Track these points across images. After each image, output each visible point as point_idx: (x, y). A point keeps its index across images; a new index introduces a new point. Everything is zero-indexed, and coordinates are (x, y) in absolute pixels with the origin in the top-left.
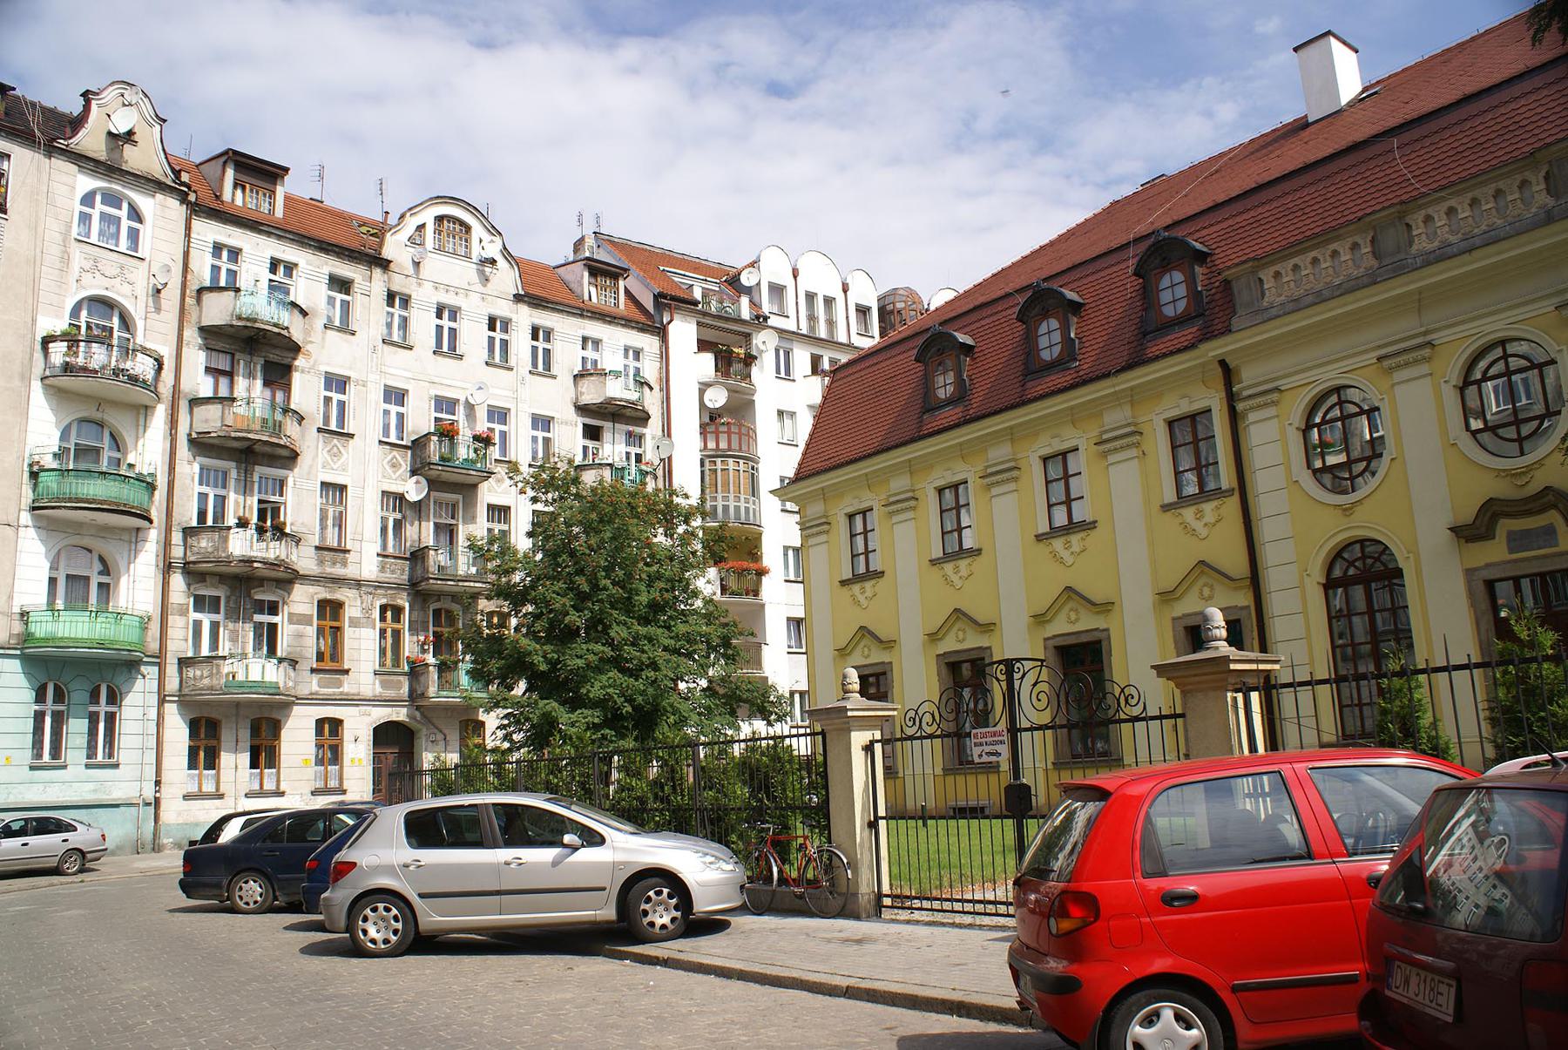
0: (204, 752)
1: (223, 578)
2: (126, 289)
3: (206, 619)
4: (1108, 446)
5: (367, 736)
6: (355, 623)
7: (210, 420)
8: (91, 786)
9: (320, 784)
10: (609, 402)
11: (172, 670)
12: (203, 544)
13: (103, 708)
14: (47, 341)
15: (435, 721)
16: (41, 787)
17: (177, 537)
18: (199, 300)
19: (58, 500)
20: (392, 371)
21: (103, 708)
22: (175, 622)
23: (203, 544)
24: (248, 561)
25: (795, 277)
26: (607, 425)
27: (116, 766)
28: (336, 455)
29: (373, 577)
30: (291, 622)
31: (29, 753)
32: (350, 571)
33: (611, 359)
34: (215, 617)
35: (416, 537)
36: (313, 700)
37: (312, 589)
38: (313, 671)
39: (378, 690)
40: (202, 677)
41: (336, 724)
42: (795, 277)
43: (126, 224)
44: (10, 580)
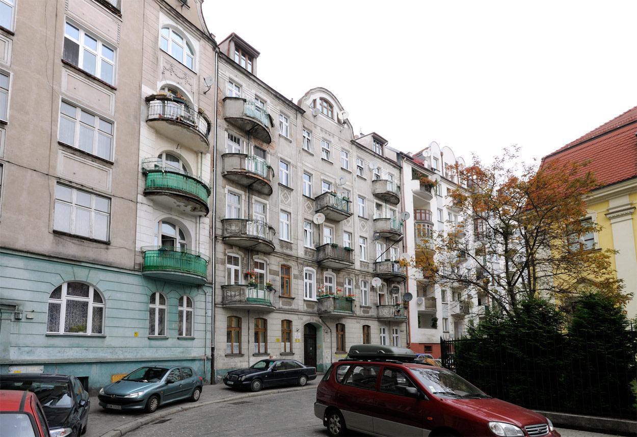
0: (234, 335)
1: (241, 248)
2: (188, 87)
3: (233, 268)
4: (611, 215)
5: (301, 328)
6: (296, 277)
7: (233, 165)
8: (181, 350)
9: (229, 352)
10: (388, 193)
11: (219, 292)
12: (233, 228)
13: (185, 309)
14: (149, 99)
15: (327, 323)
16: (155, 350)
17: (219, 225)
18: (223, 106)
19: (161, 188)
20: (306, 164)
21: (185, 309)
22: (220, 267)
23: (233, 228)
24: (256, 239)
25: (442, 156)
26: (384, 204)
27: (193, 339)
28: (286, 198)
29: (303, 257)
30: (270, 273)
31: (147, 331)
32: (293, 253)
33: (384, 176)
34: (237, 267)
35: (318, 242)
36: (280, 310)
37: (278, 259)
38: (280, 297)
39: (305, 308)
40: (235, 296)
41: (289, 322)
42: (442, 156)
43: (92, 305)
44: (133, 232)
